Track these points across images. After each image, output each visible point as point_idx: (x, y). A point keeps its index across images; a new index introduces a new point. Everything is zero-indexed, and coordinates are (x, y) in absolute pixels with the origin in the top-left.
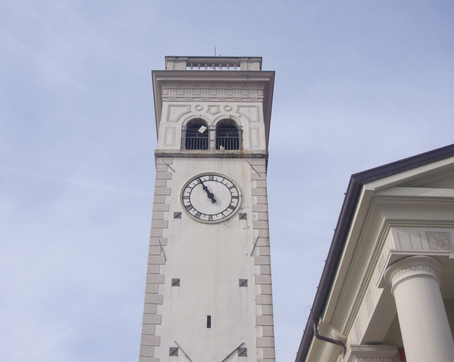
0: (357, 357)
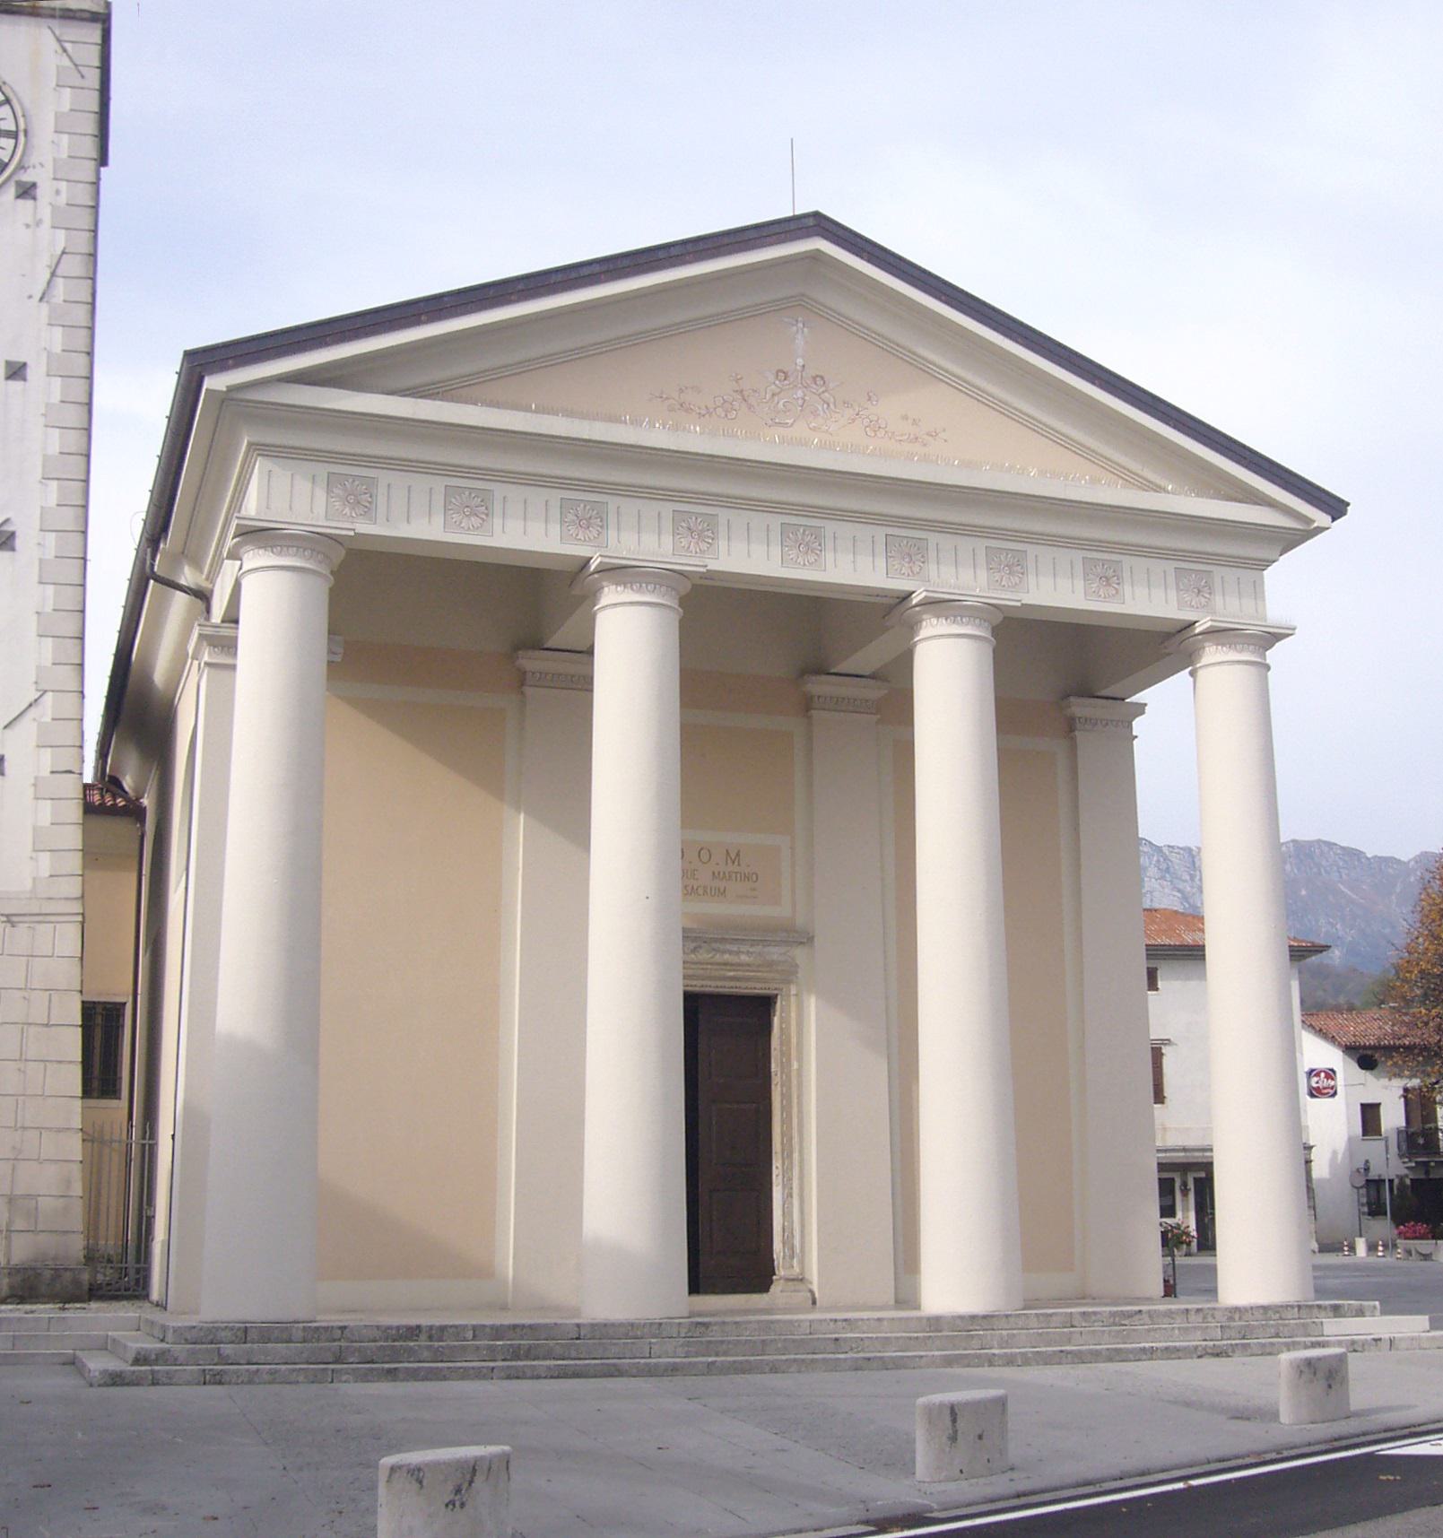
0: (210, 645)
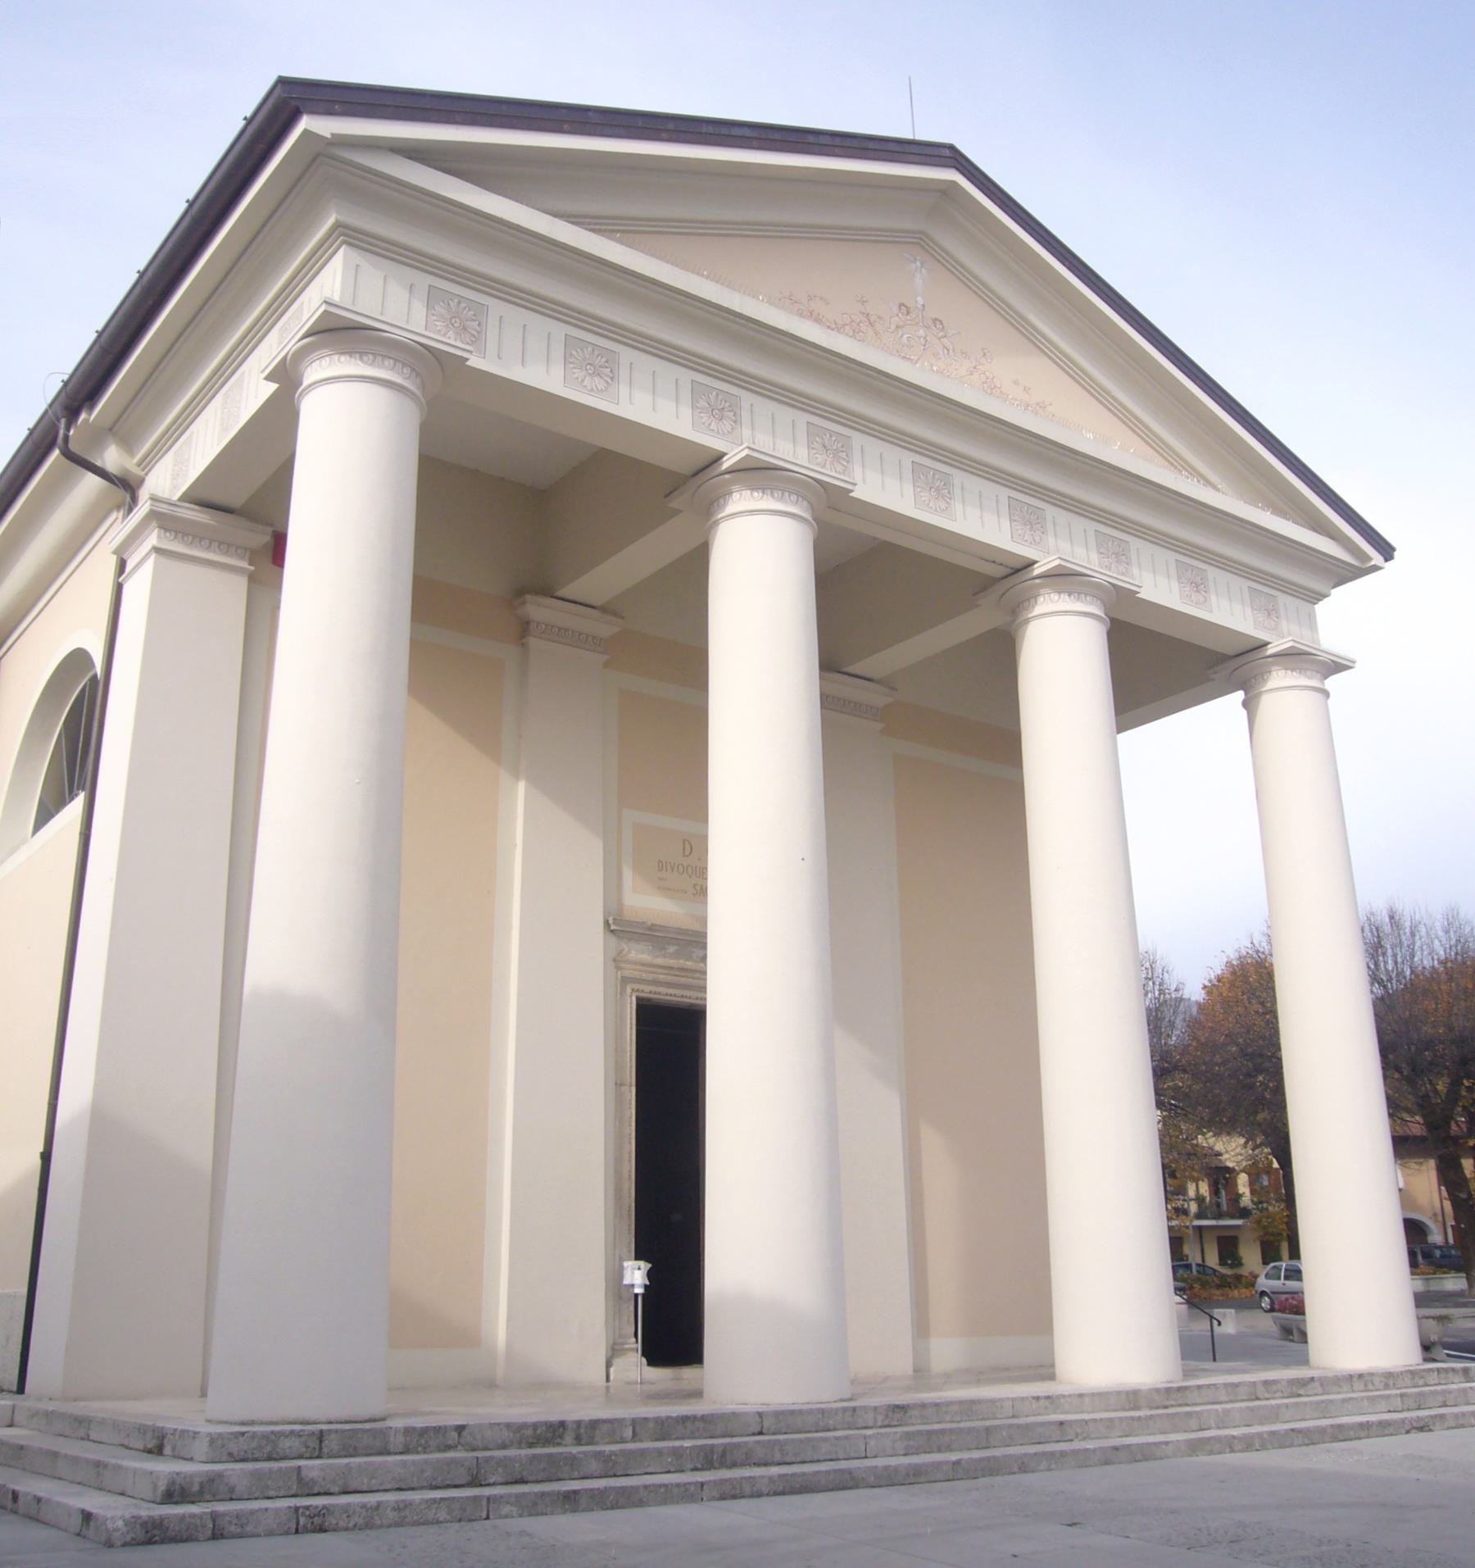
0: (160, 527)
